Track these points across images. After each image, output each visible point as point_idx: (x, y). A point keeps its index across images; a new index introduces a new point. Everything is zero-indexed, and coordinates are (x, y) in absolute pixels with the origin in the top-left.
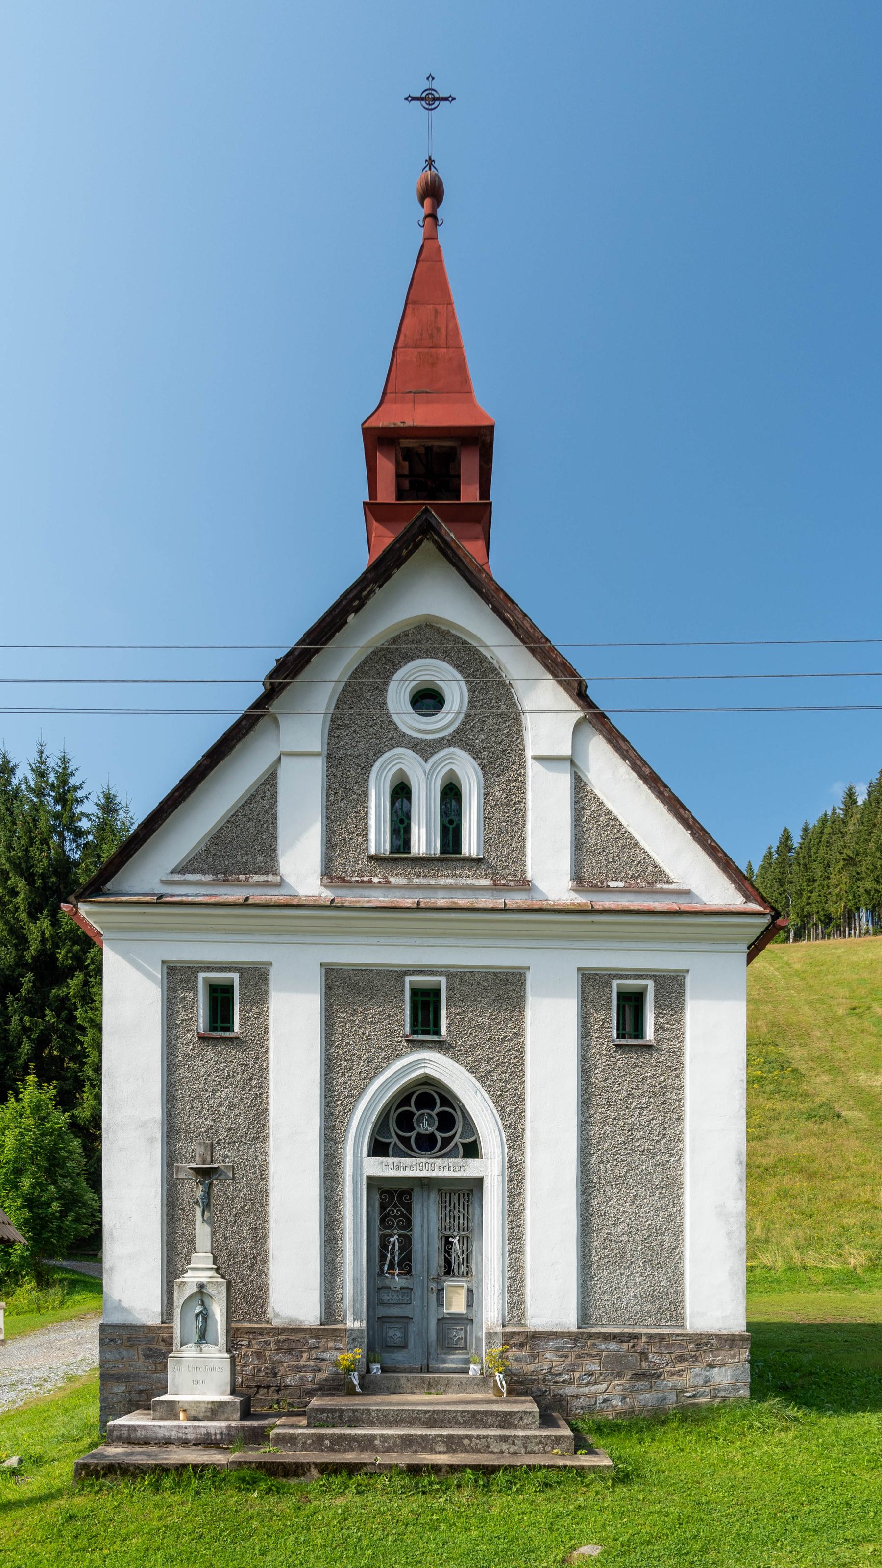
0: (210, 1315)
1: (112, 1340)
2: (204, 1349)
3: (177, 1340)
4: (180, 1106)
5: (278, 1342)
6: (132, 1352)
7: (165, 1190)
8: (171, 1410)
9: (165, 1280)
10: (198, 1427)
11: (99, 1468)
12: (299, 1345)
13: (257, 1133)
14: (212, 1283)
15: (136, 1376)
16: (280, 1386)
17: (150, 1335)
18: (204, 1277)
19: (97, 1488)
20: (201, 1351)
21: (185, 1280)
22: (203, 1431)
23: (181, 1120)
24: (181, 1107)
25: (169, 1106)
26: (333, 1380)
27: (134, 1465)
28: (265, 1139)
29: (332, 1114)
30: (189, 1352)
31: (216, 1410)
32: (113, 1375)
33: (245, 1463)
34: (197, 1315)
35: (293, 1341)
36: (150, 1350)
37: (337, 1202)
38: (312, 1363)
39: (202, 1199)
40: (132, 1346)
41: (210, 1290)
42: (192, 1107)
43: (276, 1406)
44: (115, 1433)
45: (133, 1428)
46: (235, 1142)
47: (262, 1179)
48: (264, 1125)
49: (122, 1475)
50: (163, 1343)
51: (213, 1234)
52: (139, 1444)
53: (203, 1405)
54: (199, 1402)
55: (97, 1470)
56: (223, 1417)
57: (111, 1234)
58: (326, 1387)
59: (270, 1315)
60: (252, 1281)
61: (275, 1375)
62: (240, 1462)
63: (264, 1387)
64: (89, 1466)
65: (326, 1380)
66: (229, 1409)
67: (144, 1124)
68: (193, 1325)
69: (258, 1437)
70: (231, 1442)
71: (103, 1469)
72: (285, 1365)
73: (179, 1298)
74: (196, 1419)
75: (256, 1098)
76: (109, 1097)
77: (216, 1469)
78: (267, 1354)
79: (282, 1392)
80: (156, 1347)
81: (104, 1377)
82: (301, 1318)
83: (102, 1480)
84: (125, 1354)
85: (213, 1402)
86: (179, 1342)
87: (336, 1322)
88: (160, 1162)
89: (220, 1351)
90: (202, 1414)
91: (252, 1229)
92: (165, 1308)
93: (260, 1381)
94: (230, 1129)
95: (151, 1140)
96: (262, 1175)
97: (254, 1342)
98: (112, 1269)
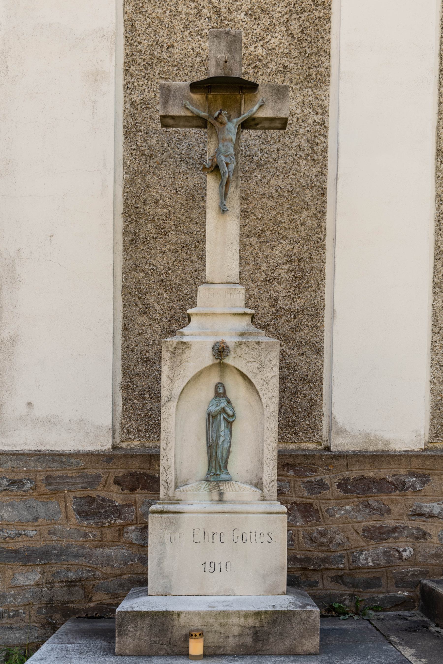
1: (13, 482)
6: (53, 505)
7: (121, 182)
9: (119, 363)
15: (62, 554)
18: (229, 329)
20: (221, 500)
21: (185, 339)
36: (91, 500)
40: (54, 493)
50: (116, 488)
53: (235, 620)
56: (281, 647)
73: (172, 380)
80: (103, 494)
84: (41, 510)
85: (257, 614)
92: (119, 419)
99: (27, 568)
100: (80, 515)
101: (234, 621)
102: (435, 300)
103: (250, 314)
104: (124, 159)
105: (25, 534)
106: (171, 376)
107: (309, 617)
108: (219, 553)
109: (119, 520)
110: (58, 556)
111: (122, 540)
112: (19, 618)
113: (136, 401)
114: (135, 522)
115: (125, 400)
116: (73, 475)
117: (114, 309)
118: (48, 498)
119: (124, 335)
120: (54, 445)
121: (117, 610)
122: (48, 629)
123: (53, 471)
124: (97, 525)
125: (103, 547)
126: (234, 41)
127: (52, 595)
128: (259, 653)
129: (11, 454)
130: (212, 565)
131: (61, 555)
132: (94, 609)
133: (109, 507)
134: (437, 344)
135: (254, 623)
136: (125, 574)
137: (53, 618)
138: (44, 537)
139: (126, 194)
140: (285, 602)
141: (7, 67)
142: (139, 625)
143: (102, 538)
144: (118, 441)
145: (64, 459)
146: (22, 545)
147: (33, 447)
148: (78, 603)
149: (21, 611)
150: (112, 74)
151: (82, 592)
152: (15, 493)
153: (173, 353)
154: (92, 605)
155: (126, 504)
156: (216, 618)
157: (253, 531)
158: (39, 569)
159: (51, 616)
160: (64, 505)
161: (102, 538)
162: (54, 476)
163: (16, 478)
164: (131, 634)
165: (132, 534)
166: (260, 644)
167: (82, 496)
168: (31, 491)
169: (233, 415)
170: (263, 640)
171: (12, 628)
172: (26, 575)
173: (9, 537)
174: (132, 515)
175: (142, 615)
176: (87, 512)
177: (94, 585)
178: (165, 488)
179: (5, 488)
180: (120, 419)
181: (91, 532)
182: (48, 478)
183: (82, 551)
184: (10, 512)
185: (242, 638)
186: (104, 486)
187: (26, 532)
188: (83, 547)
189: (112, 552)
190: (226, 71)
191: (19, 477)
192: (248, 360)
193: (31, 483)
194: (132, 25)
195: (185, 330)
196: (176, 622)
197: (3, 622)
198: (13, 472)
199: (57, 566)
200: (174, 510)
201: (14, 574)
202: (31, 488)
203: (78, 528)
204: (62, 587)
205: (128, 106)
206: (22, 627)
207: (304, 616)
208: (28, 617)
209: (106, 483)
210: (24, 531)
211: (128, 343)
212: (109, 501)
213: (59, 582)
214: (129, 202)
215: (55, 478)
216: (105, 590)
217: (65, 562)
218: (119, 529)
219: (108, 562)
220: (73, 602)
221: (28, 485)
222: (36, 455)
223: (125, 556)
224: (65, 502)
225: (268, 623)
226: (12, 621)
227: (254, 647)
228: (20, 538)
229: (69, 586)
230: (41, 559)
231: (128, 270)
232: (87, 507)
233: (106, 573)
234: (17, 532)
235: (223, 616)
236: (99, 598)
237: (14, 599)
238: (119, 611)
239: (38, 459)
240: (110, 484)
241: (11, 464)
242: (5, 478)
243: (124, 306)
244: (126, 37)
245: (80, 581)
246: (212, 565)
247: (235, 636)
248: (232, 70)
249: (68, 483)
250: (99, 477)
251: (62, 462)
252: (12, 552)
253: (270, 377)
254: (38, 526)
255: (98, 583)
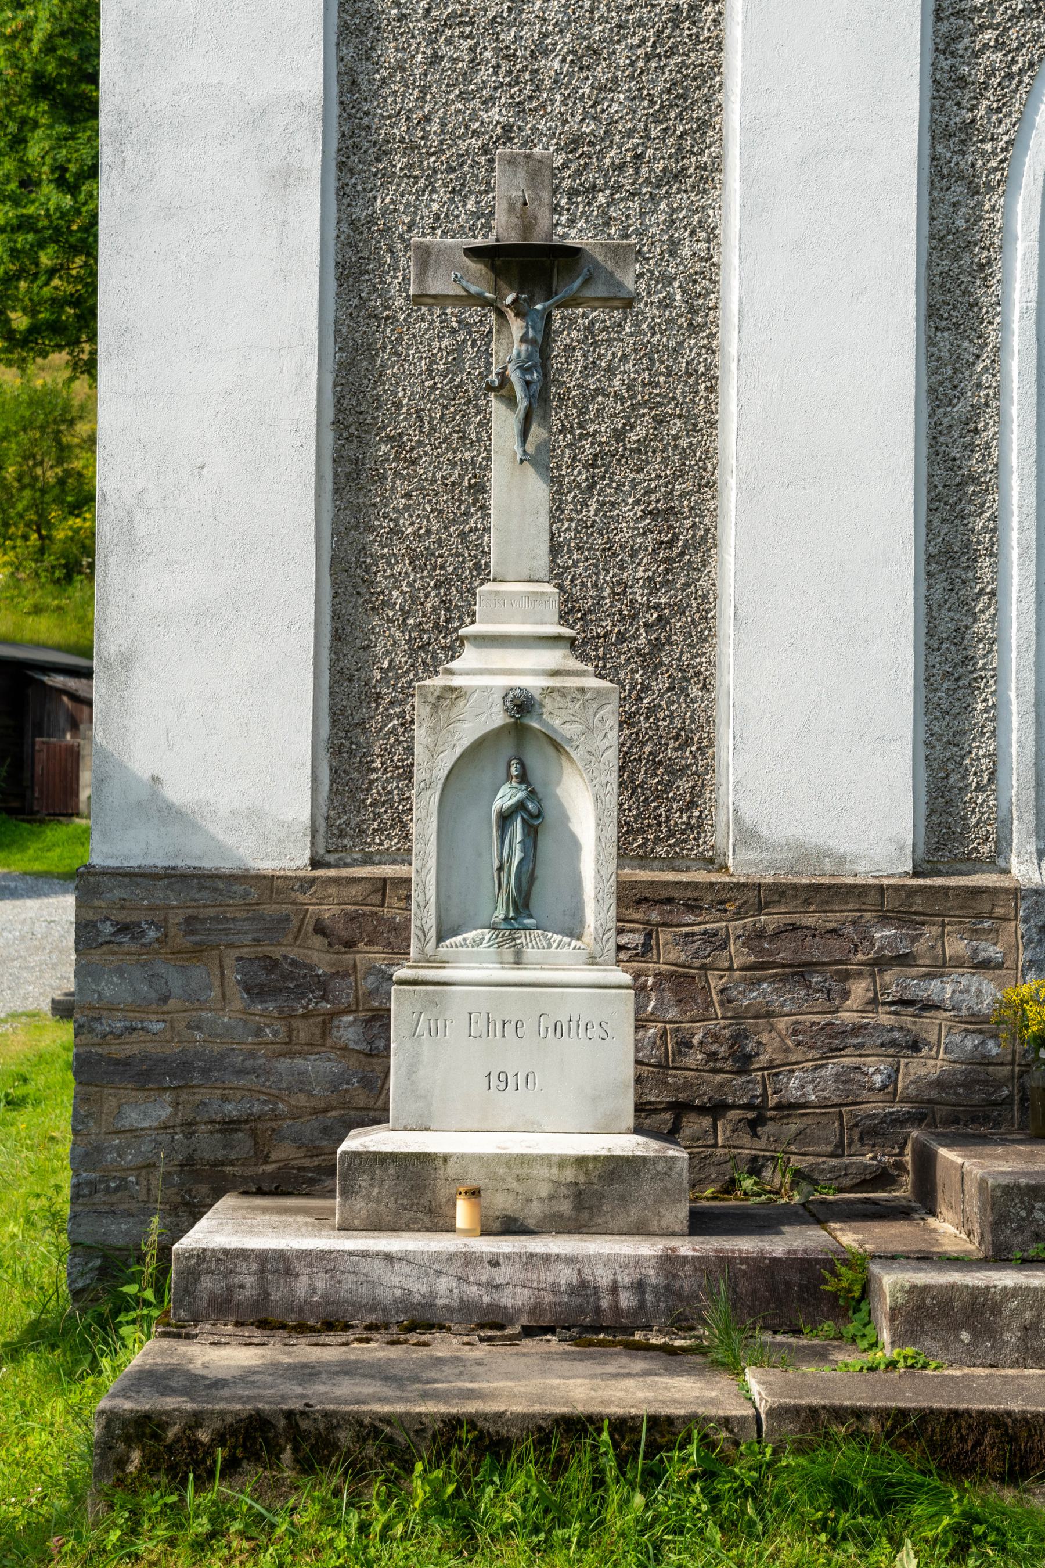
0: (550, 814)
1: (124, 928)
2: (531, 953)
3: (423, 914)
4: (389, 53)
5: (755, 937)
6: (198, 974)
7: (330, 365)
8: (415, 1190)
9: (325, 702)
10: (546, 1258)
11: (203, 1436)
12: (837, 948)
13: (680, 153)
14: (562, 692)
16: (762, 1107)
17: (270, 909)
18: (529, 670)
19: (202, 1526)
21: (456, 681)
22: (566, 1276)
23: (395, 109)
24: (392, 57)
25: (347, 52)
26: (968, 1084)
27: (357, 1421)
28: (709, 174)
29: (962, 82)
30: (473, 963)
31: (594, 1194)
32: (125, 1063)
33: (839, 1414)
34: (505, 819)
35: (813, 932)
36: (271, 964)
37: (976, 412)
38: (884, 1018)
39: (524, 370)
40: (199, 950)
41: (556, 719)
42: (435, 59)
43: (748, 1184)
44: (208, 1284)
45: (277, 1265)
46: (594, 188)
47: (693, 328)
48: (704, 125)
49: (305, 1466)
50: (318, 941)
51: (556, 513)
52: (302, 1328)
53: (543, 1172)
54: (524, 1160)
55: (195, 1445)
56: (622, 1221)
57: (128, 530)
58: (941, 1111)
59: (723, 835)
60: (652, 710)
61: (744, 1062)
62: (813, 1411)
63: (702, 1110)
64: (164, 1426)
65: (939, 1084)
66: (648, 1188)
67: (257, 118)
68: (495, 853)
69: (810, 1301)
70: (682, 1324)
71: (220, 1438)
72: (782, 1024)
73: (433, 753)
74: (511, 1227)
75: (676, 24)
76: (127, 13)
77: (715, 1444)
78: (715, 982)
79: (771, 1128)
80: (293, 953)
81: (90, 1070)
82: (842, 848)
83: (219, 1488)
84: (175, 981)
85: (581, 1161)
86: (431, 921)
87: (971, 863)
88: (316, 258)
89: (592, 961)
90: (536, 1211)
91: (654, 514)
93: (687, 1085)
94: (576, 141)
95: (284, 179)
96: (693, 310)
97: (664, 936)
98: (127, 660)
99: (146, 1093)
100: (248, 993)
101: (541, 1172)
102: (930, 587)
103: (570, 638)
104: (336, 323)
105: (143, 1029)
106: (431, 747)
107: (671, 1169)
108: (514, 1058)
109: (324, 1004)
110: (205, 1072)
111: (329, 1042)
112: (127, 1193)
113: (355, 775)
114: (354, 1008)
115: (335, 772)
116: (238, 915)
117: (317, 602)
118: (188, 959)
119: (334, 650)
120: (200, 858)
121: (339, 1151)
122: (184, 1216)
123: (198, 907)
124: (281, 1012)
125: (291, 1055)
126: (540, 169)
127: (193, 1147)
128: (584, 1230)
129: (120, 874)
130: (502, 1077)
131: (210, 1070)
132: (272, 1176)
133: (304, 977)
134: (935, 671)
135: (576, 1177)
136: (334, 1109)
137: (194, 1193)
138: (179, 1034)
139: (339, 389)
140: (630, 1144)
141: (124, 161)
142: (377, 1177)
143: (290, 1037)
144: (322, 851)
145: (221, 885)
146: (135, 1049)
147: (160, 860)
148: (243, 1164)
149: (132, 1179)
150: (317, 174)
151: (250, 1143)
152: (126, 948)
153: (435, 707)
154: (269, 1168)
155: (338, 972)
156: (509, 1167)
157: (575, 1019)
158: (168, 1096)
159: (190, 1190)
160: (218, 973)
161: (290, 1037)
162: (201, 916)
163: (129, 920)
164: (364, 1192)
165: (348, 1031)
166: (585, 1215)
167: (253, 956)
168: (157, 946)
169: (539, 815)
170: (591, 1208)
171: (113, 1212)
172: (142, 1107)
173: (111, 1033)
174: (348, 994)
175: (383, 1159)
176: (261, 986)
177: (274, 1130)
178: (420, 940)
179: (108, 939)
180: (325, 809)
181: (268, 1026)
182: (189, 920)
183: (251, 1062)
184: (117, 985)
185: (554, 1202)
186: (296, 938)
187: (146, 1024)
188: (253, 1055)
189: (309, 1064)
190: (526, 221)
191: (135, 919)
192: (565, 719)
193: (158, 929)
194: (354, 82)
195: (454, 665)
196: (441, 1172)
197: (96, 1201)
198: (123, 908)
199: (203, 1090)
200: (436, 979)
201: (120, 1106)
202: (157, 939)
203: (245, 1017)
204: (211, 1133)
205: (344, 227)
206: (134, 1211)
207: (661, 1166)
208: (144, 1192)
209: (299, 931)
210: (142, 1022)
211: (341, 664)
212: (304, 965)
213: (206, 1123)
214: (346, 402)
215: (203, 921)
216: (294, 1141)
217: (219, 1084)
218: (324, 1022)
219: (301, 1083)
220: (232, 1163)
221: (152, 934)
222: (167, 876)
223: (335, 1074)
224: (222, 967)
225: (600, 1177)
226: (114, 1199)
227: (576, 1220)
228: (134, 1035)
229: (226, 1130)
230: (173, 1076)
231: (342, 529)
232: (262, 977)
233: (296, 1107)
234: (128, 1024)
235: (522, 1163)
236: (283, 1156)
237: (120, 1156)
238: (345, 1153)
239: (171, 883)
240: (306, 933)
241: (118, 893)
242: (108, 919)
243: (336, 595)
244: (342, 103)
245: (247, 1121)
246: (502, 1077)
247: (542, 1200)
248: (536, 218)
249: (227, 931)
250: (287, 919)
251: (216, 890)
252: (118, 1062)
253: (602, 749)
254: (168, 1013)
255: (281, 1126)
